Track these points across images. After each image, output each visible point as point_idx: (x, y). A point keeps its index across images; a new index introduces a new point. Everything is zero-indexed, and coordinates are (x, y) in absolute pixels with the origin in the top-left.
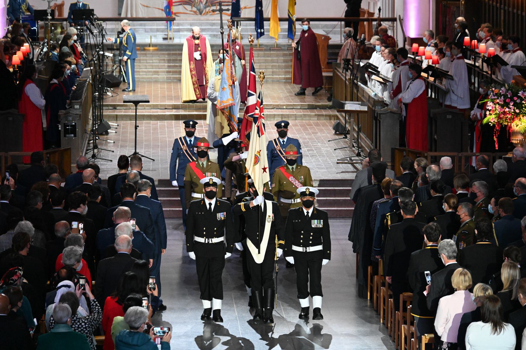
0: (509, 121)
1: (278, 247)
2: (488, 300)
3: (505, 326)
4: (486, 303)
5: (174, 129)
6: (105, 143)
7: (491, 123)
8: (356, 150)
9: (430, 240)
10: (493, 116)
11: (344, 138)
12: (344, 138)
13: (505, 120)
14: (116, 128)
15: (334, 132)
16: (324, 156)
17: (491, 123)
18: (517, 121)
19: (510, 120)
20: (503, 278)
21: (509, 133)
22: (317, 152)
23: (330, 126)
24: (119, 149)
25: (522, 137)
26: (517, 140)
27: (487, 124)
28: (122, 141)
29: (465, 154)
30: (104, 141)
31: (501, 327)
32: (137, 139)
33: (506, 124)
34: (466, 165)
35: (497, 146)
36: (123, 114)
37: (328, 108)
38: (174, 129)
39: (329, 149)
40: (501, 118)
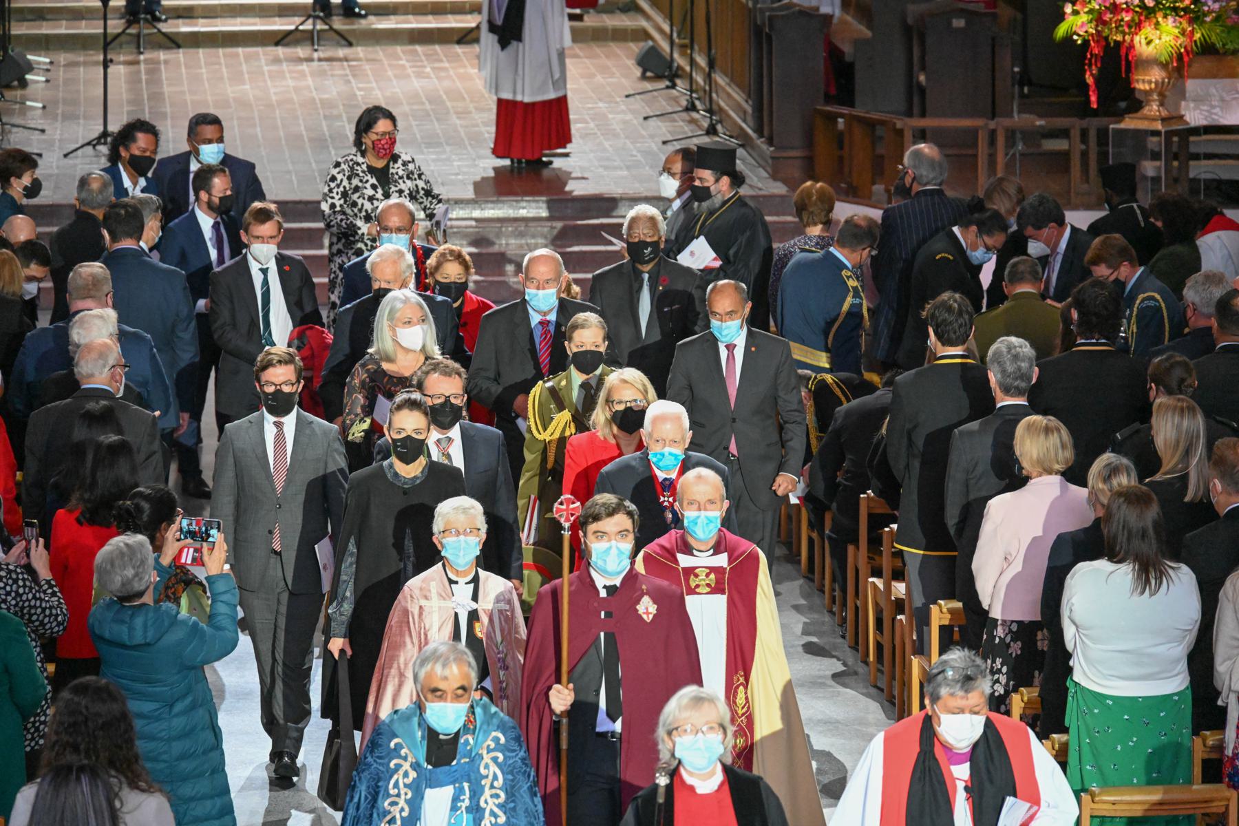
0: (1127, 30)
1: (461, 408)
2: (1122, 500)
3: (1171, 571)
4: (1119, 507)
5: (204, 70)
6: (20, 109)
7: (1079, 35)
8: (702, 117)
9: (945, 341)
10: (1084, 18)
11: (668, 87)
12: (668, 87)
13: (1117, 28)
14: (48, 70)
15: (638, 72)
16: (616, 136)
17: (1079, 35)
18: (1148, 31)
19: (1129, 26)
20: (1160, 442)
21: (1128, 63)
22: (597, 126)
23: (628, 58)
24: (58, 124)
25: (1164, 74)
26: (1150, 82)
27: (1068, 39)
28: (65, 102)
29: (1006, 122)
30: (16, 103)
31: (1162, 573)
32: (109, 97)
33: (1119, 38)
34: (1007, 154)
35: (1093, 98)
36: (63, 31)
37: (619, 9)
38: (204, 70)
39: (629, 117)
40: (1105, 23)
